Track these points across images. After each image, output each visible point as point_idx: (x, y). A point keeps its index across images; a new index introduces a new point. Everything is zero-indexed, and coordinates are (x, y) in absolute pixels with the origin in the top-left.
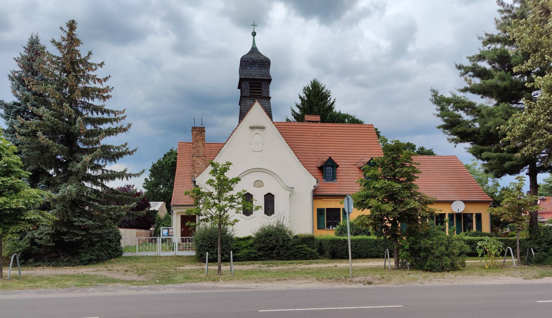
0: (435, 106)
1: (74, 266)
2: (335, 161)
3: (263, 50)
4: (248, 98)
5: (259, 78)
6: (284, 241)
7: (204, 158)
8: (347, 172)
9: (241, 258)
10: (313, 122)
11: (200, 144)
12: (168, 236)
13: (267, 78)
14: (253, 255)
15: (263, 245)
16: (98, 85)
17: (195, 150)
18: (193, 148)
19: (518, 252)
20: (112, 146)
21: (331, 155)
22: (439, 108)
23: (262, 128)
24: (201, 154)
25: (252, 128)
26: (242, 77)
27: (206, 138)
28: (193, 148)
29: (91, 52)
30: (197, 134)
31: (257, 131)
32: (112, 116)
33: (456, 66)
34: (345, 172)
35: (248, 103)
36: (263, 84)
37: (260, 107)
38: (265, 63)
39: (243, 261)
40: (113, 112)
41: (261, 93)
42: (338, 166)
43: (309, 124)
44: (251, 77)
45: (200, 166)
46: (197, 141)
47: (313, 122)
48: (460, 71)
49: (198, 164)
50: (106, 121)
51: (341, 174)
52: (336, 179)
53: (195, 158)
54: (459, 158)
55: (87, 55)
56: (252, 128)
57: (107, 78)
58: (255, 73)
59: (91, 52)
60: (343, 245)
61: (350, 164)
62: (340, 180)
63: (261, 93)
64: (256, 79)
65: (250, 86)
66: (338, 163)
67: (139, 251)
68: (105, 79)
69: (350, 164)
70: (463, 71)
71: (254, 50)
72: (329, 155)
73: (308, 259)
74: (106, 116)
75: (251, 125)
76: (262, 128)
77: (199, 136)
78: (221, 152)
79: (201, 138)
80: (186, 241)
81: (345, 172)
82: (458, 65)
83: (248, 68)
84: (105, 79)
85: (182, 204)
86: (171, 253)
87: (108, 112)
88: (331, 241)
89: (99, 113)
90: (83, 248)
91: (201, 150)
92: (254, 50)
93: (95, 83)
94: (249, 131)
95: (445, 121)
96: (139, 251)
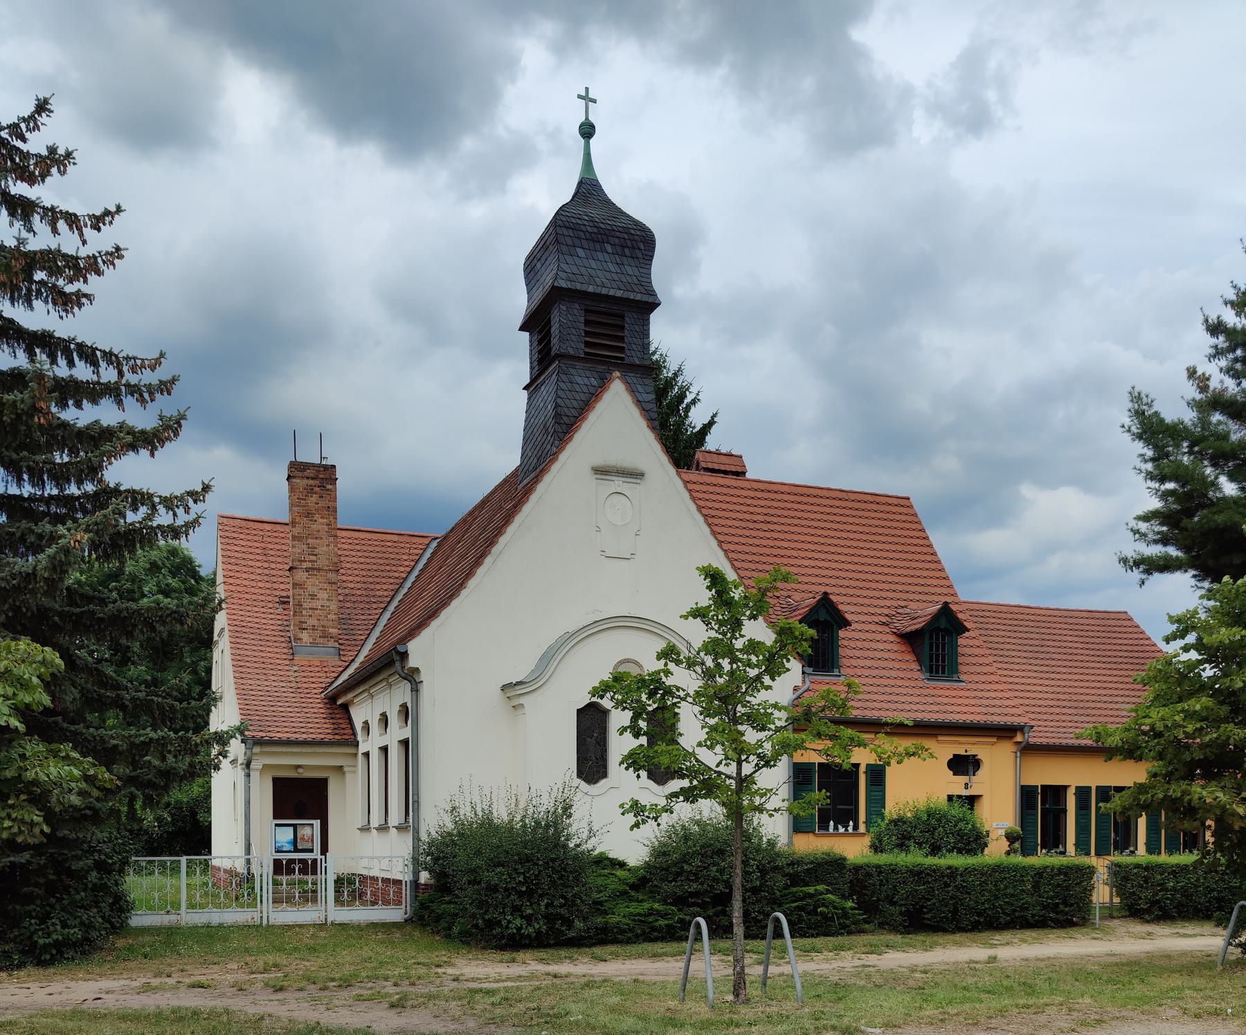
0: (1139, 447)
1: (484, 948)
2: (841, 607)
3: (626, 191)
4: (579, 365)
5: (619, 294)
6: (763, 871)
7: (332, 576)
8: (866, 645)
9: (622, 932)
10: (726, 472)
11: (320, 524)
12: (296, 850)
13: (645, 298)
14: (662, 922)
15: (695, 886)
16: (68, 242)
17: (300, 548)
18: (294, 538)
19: (692, 930)
20: (151, 496)
21: (829, 590)
22: (1150, 453)
23: (635, 475)
24: (322, 562)
25: (602, 472)
26: (563, 284)
27: (339, 504)
28: (294, 538)
29: (46, 101)
30: (310, 491)
31: (618, 484)
32: (108, 374)
33: (1207, 320)
34: (859, 644)
35: (579, 380)
36: (629, 319)
37: (627, 399)
38: (636, 242)
39: (628, 942)
40: (110, 357)
41: (622, 350)
42: (846, 623)
43: (708, 478)
44: (591, 289)
45: (318, 604)
46: (308, 515)
47: (726, 472)
48: (1214, 341)
49: (313, 596)
50: (94, 392)
51: (850, 653)
52: (839, 667)
53: (300, 576)
54: (1138, 620)
55: (28, 109)
56: (602, 472)
57: (107, 213)
58: (599, 274)
59: (46, 101)
60: (947, 885)
61: (869, 619)
62: (851, 671)
63: (622, 350)
64: (607, 296)
65: (587, 322)
66: (849, 617)
67: (192, 906)
68: (98, 222)
69: (869, 619)
70: (1221, 341)
71: (588, 189)
72: (823, 589)
73: (832, 935)
74: (83, 372)
75: (599, 461)
76: (635, 475)
77: (314, 498)
78: (495, 550)
79: (322, 503)
80: (290, 871)
81: (859, 644)
82: (1213, 318)
83: (580, 252)
84: (98, 222)
85: (284, 736)
86: (306, 915)
87: (89, 354)
88: (911, 872)
89: (62, 362)
90: (30, 899)
91: (325, 550)
92: (588, 189)
93: (55, 231)
94: (591, 479)
95: (1165, 495)
96: (192, 906)
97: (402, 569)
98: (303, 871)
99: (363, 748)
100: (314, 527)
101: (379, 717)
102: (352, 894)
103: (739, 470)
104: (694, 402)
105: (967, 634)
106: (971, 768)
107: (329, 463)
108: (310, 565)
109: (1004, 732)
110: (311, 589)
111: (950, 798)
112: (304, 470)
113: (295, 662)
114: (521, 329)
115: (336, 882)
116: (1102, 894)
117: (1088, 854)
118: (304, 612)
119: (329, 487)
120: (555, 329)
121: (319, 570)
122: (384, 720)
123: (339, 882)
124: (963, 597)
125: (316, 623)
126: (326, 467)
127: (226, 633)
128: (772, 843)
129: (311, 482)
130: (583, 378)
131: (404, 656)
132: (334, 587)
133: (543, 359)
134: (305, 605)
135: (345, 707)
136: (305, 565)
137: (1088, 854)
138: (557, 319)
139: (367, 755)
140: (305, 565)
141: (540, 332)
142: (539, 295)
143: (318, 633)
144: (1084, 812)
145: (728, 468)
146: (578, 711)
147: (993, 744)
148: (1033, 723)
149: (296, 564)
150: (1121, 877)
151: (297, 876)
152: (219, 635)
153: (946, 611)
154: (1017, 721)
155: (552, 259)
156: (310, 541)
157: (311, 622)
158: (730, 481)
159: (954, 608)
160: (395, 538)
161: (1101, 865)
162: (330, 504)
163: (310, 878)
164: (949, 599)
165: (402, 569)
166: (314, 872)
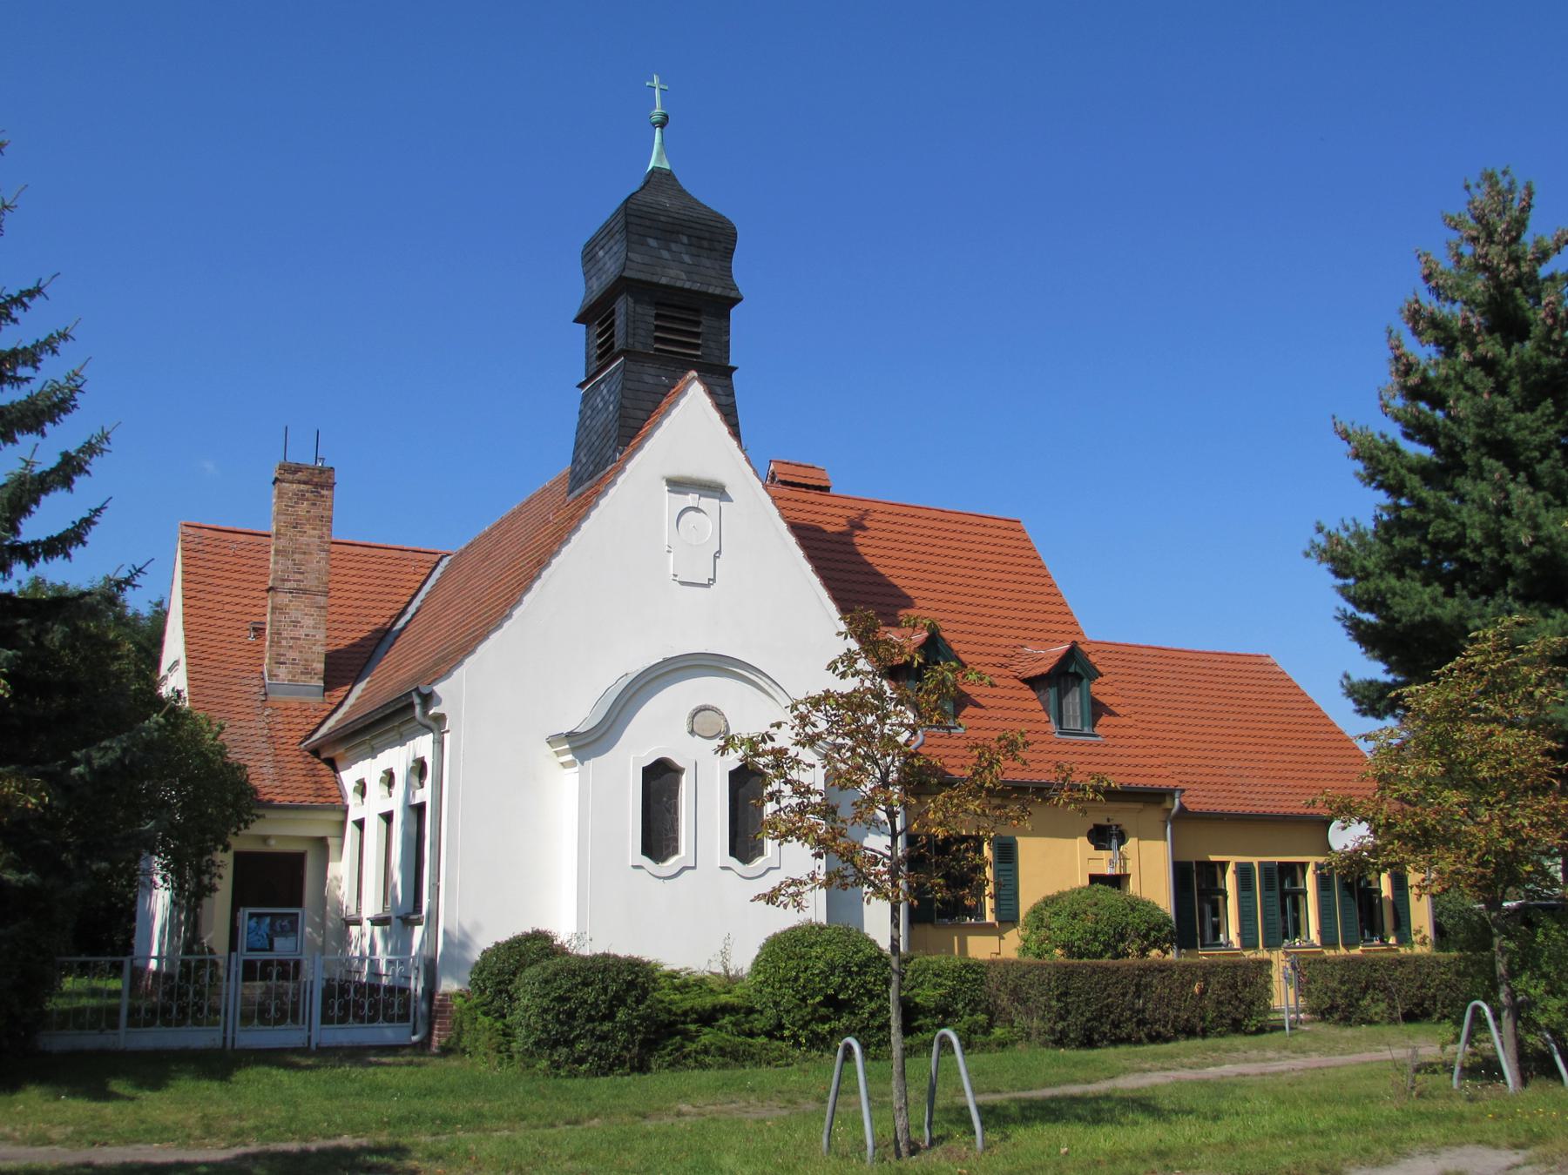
7: (322, 600)
11: (310, 536)
13: (726, 293)
23: (716, 490)
24: (310, 582)
25: (677, 485)
30: (302, 497)
45: (302, 633)
49: (296, 623)
56: (677, 485)
76: (716, 490)
97: (404, 591)
98: (283, 976)
99: (353, 815)
100: (305, 539)
101: (381, 775)
102: (345, 1007)
103: (823, 484)
104: (581, 386)
105: (1100, 679)
106: (1114, 842)
107: (328, 464)
108: (295, 585)
109: (1154, 797)
110: (295, 615)
111: (1094, 879)
112: (295, 472)
113: (268, 704)
114: (576, 321)
115: (324, 990)
116: (1283, 997)
117: (1256, 946)
118: (284, 643)
119: (324, 492)
120: (620, 321)
121: (305, 591)
122: (389, 778)
123: (328, 993)
124: (1089, 636)
125: (295, 655)
126: (322, 471)
127: (182, 667)
128: (136, 615)
129: (302, 487)
130: (650, 375)
131: (428, 699)
132: (323, 612)
133: (604, 353)
134: (285, 634)
135: (331, 763)
136: (288, 585)
137: (1256, 946)
138: (622, 306)
139: (360, 824)
140: (288, 585)
141: (600, 325)
142: (598, 286)
143: (300, 669)
144: (1246, 894)
145: (810, 482)
146: (644, 769)
147: (1141, 811)
148: (1182, 786)
149: (277, 584)
150: (1306, 972)
151: (273, 982)
152: (170, 670)
153: (1073, 654)
154: (1164, 783)
155: (618, 247)
156: (296, 556)
157: (291, 654)
158: (812, 496)
159: (1083, 647)
160: (397, 554)
161: (1279, 961)
162: (326, 513)
163: (290, 986)
164: (1076, 638)
165: (404, 591)
166: (296, 977)
